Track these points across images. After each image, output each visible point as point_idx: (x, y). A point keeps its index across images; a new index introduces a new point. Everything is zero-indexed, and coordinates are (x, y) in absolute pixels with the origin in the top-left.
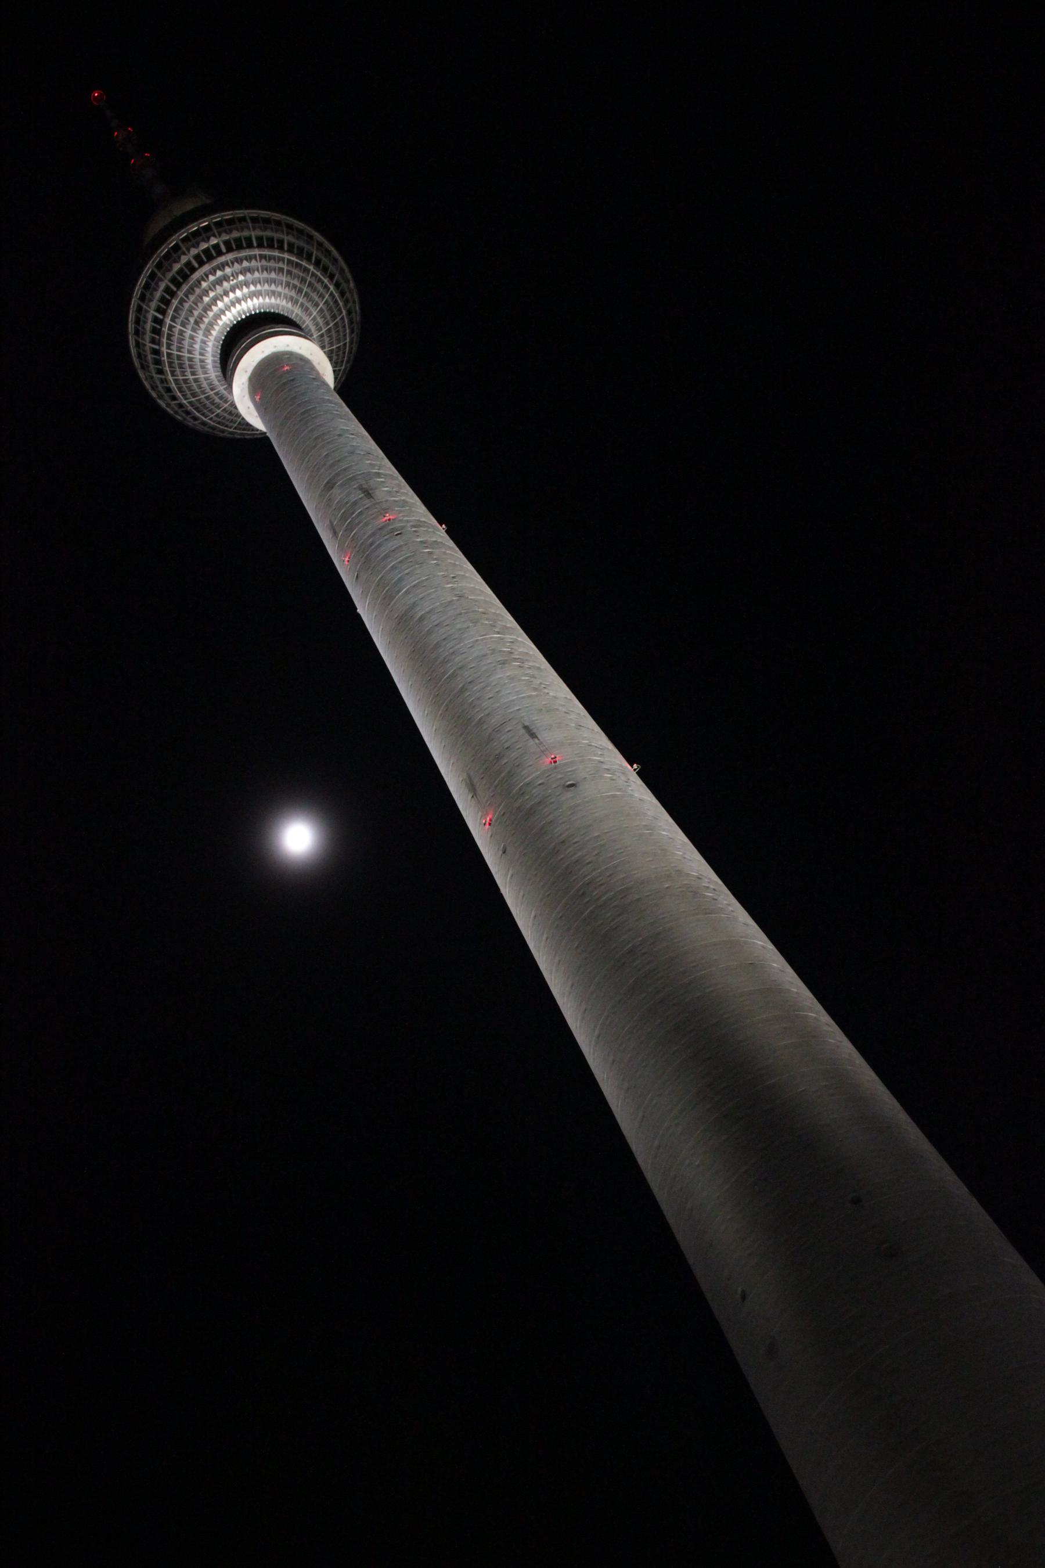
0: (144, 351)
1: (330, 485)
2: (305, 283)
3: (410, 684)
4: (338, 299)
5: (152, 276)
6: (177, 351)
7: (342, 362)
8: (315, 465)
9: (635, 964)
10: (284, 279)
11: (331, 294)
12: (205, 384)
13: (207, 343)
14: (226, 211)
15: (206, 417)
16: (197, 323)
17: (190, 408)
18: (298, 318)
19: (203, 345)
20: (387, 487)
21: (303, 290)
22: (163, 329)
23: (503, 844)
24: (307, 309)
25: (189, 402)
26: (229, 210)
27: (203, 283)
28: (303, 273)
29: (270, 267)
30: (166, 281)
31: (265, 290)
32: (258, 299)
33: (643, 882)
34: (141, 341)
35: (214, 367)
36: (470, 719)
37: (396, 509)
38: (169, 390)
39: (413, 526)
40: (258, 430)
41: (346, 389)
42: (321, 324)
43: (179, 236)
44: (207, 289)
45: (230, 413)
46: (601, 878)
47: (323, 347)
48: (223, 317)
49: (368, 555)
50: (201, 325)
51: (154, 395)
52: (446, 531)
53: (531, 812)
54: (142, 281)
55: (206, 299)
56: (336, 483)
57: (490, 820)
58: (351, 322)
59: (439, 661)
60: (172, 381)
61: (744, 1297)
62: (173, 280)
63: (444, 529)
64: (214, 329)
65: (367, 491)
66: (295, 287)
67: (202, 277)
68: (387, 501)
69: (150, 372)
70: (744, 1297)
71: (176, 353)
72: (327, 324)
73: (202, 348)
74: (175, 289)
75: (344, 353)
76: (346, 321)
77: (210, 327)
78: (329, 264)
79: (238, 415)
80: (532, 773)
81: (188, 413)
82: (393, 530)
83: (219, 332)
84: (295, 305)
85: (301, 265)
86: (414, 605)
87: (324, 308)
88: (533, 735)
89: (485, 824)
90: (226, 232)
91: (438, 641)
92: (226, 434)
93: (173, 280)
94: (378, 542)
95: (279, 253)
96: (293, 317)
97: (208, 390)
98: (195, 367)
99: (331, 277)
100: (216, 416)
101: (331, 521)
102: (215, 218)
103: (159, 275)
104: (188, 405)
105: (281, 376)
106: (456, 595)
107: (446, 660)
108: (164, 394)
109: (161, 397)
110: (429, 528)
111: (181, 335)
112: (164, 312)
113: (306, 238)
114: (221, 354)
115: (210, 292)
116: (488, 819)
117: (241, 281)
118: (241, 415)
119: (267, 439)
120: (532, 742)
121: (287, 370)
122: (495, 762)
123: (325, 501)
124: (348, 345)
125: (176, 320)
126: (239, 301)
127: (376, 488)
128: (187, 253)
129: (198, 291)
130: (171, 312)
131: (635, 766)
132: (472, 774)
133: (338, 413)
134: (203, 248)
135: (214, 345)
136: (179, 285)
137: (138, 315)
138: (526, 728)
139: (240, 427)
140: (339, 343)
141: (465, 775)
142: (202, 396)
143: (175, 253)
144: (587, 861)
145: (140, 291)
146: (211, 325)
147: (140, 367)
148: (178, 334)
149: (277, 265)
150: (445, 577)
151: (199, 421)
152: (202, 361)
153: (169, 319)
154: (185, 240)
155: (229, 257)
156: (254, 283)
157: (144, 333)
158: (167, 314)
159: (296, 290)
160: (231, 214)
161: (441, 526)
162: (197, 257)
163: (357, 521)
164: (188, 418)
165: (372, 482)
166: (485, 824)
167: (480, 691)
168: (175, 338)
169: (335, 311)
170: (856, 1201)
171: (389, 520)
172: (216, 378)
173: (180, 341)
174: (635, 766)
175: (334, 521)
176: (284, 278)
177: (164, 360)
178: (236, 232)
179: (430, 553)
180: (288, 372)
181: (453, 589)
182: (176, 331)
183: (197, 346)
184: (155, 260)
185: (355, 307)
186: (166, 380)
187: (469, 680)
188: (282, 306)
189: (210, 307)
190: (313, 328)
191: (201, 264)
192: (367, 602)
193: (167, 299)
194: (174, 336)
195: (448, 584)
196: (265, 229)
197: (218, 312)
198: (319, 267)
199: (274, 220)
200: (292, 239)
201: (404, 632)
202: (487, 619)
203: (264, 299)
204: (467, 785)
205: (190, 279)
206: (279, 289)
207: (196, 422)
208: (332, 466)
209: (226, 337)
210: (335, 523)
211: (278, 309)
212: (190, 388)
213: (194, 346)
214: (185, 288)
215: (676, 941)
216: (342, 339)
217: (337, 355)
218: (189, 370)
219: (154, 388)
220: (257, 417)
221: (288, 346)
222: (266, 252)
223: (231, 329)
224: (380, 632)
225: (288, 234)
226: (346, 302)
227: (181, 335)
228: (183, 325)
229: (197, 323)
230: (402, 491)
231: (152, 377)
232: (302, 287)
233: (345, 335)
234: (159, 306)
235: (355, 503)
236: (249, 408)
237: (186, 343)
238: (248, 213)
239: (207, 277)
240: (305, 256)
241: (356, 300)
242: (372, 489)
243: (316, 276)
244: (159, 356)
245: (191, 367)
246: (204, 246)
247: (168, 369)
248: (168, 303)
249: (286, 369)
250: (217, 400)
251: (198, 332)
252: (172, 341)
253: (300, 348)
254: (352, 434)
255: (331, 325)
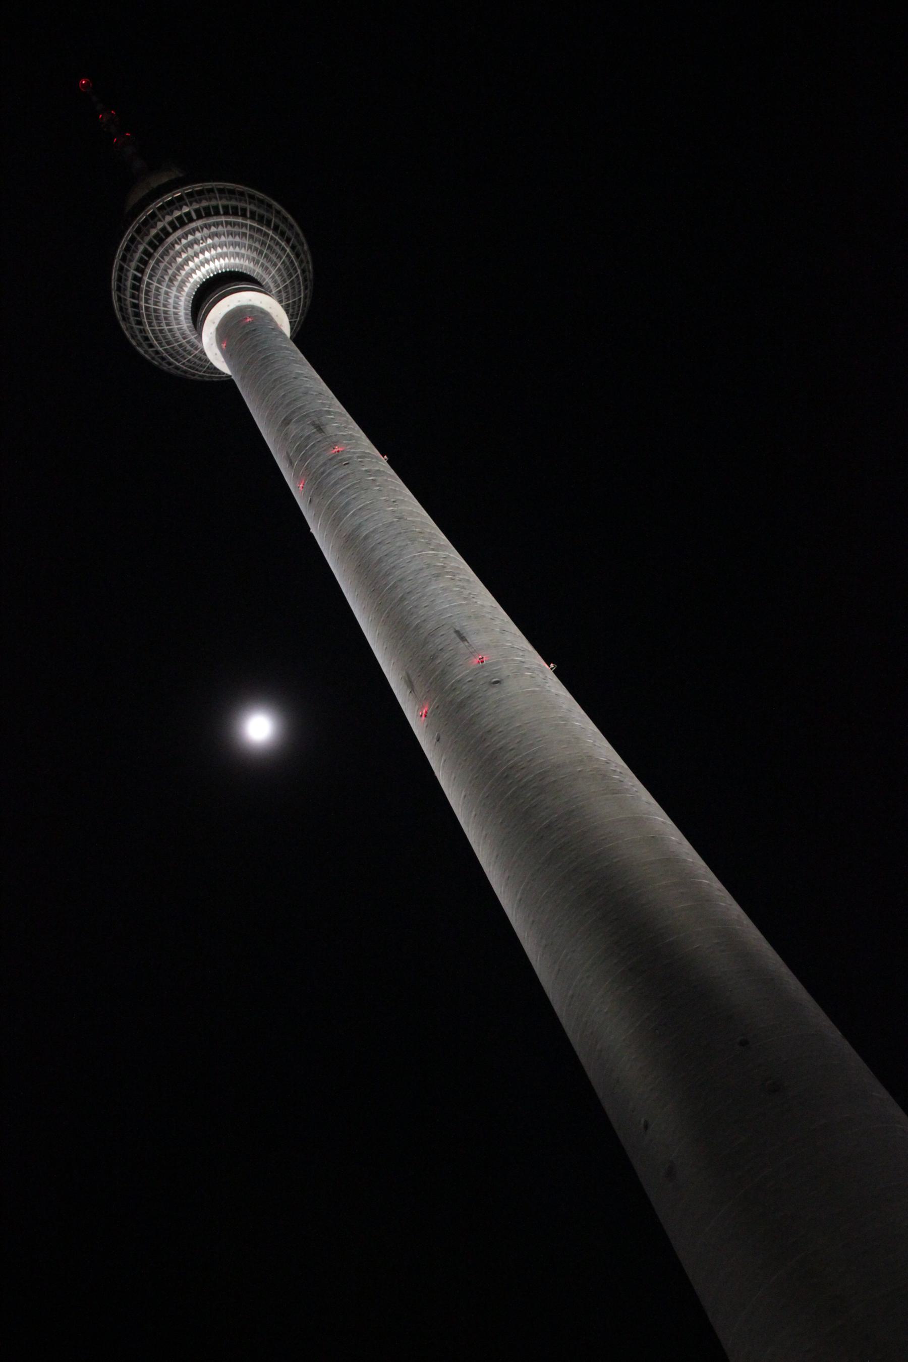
0: (125, 304)
1: (287, 422)
2: (265, 246)
3: (356, 594)
4: (294, 260)
5: (132, 240)
6: (154, 305)
7: (297, 314)
8: (274, 404)
9: (552, 837)
10: (247, 243)
11: (288, 256)
12: (178, 333)
13: (180, 298)
14: (196, 183)
15: (179, 362)
16: (171, 280)
17: (165, 354)
18: (259, 277)
19: (176, 299)
20: (336, 423)
21: (263, 252)
22: (142, 286)
23: (437, 733)
24: (267, 269)
25: (164, 350)
26: (199, 183)
27: (176, 246)
28: (263, 237)
29: (235, 232)
30: (144, 244)
31: (230, 252)
32: (224, 259)
33: (558, 766)
34: (122, 296)
35: (186, 319)
36: (408, 624)
37: (344, 442)
38: (147, 339)
39: (359, 457)
40: (224, 373)
41: (300, 338)
42: (279, 282)
43: (155, 205)
44: (180, 251)
45: (200, 359)
46: (522, 763)
47: (280, 302)
48: (193, 275)
49: (320, 482)
50: (175, 283)
51: (134, 343)
52: (387, 461)
53: (461, 705)
54: (123, 244)
55: (179, 260)
56: (292, 419)
57: (426, 712)
58: (305, 280)
59: (381, 574)
60: (150, 331)
61: (646, 1127)
62: (151, 243)
63: (385, 459)
64: (186, 286)
65: (319, 426)
66: (256, 249)
67: (176, 241)
68: (336, 435)
69: (130, 324)
70: (646, 1127)
71: (153, 306)
72: (284, 281)
73: (176, 303)
74: (152, 251)
75: (299, 307)
76: (301, 279)
77: (183, 284)
78: (286, 229)
79: (207, 361)
80: (462, 672)
81: (163, 359)
82: (341, 461)
83: (190, 288)
84: (256, 265)
85: (261, 230)
86: (360, 525)
87: (282, 267)
88: (463, 639)
89: (421, 716)
90: (196, 201)
91: (381, 557)
92: (196, 377)
93: (151, 243)
94: (328, 471)
95: (242, 219)
96: (254, 275)
97: (181, 339)
98: (169, 318)
99: (288, 241)
100: (188, 361)
101: (287, 453)
102: (187, 189)
103: (138, 239)
104: (163, 352)
105: (244, 327)
106: (396, 517)
107: (387, 574)
108: (143, 342)
109: (140, 345)
110: (372, 458)
111: (158, 291)
112: (142, 271)
113: (265, 207)
114: (192, 308)
115: (182, 253)
116: (424, 712)
117: (209, 244)
118: (209, 361)
119: (232, 381)
120: (462, 645)
121: (249, 321)
122: (430, 662)
123: (282, 435)
124: (302, 300)
125: (153, 278)
126: (207, 261)
127: (327, 424)
128: (162, 219)
129: (172, 253)
130: (148, 271)
131: (552, 665)
132: (410, 672)
133: (294, 359)
134: (176, 216)
135: (186, 300)
136: (155, 248)
137: (120, 273)
138: (457, 632)
139: (209, 371)
140: (295, 298)
141: (404, 673)
142: (176, 344)
143: (152, 220)
144: (510, 748)
145: (122, 253)
146: (183, 282)
147: (121, 319)
148: (155, 290)
149: (241, 230)
150: (386, 501)
151: (173, 366)
152: (175, 314)
153: (147, 277)
154: (161, 208)
155: (199, 223)
156: (221, 246)
157: (125, 290)
158: (145, 272)
159: (257, 252)
160: (201, 186)
161: (383, 457)
162: (171, 224)
163: (310, 453)
164: (163, 363)
165: (323, 419)
166: (421, 716)
167: (417, 600)
168: (152, 294)
169: (291, 271)
170: (744, 1043)
171: (338, 451)
172: (188, 328)
173: (157, 296)
174: (552, 665)
175: (291, 453)
176: (247, 242)
177: (143, 313)
178: (205, 201)
179: (373, 480)
180: (250, 323)
181: (393, 511)
182: (153, 287)
183: (171, 301)
184: (134, 225)
185: (308, 267)
186: (144, 330)
187: (408, 590)
188: (245, 266)
189: (183, 266)
190: (272, 285)
191: (175, 229)
192: (319, 523)
193: (145, 260)
194: (152, 292)
195: (389, 507)
196: (231, 199)
197: (190, 271)
198: (277, 232)
199: (238, 191)
200: (254, 208)
201: (351, 549)
202: (423, 538)
203: (229, 259)
204: (406, 682)
205: (165, 242)
206: (243, 251)
207: (171, 367)
208: (288, 405)
209: (196, 292)
210: (291, 455)
211: (242, 268)
212: (165, 337)
213: (169, 300)
214: (161, 250)
215: (587, 817)
216: (297, 295)
217: (293, 309)
218: (164, 322)
219: (134, 337)
220: (223, 362)
221: (250, 300)
222: (231, 219)
223: (201, 285)
224: (330, 549)
225: (250, 203)
226: (301, 262)
227: (158, 291)
228: (159, 282)
229: (171, 280)
230: (350, 426)
231: (132, 328)
232: (263, 249)
233: (300, 291)
234: (138, 266)
235: (309, 437)
236: (216, 354)
237: (162, 298)
238: (216, 185)
239: (180, 241)
240: (265, 222)
241: (310, 260)
242: (323, 425)
243: (275, 240)
244: (139, 309)
245: (166, 319)
246: (177, 213)
247: (146, 321)
248: (146, 263)
249: (248, 320)
250: (189, 348)
251: (172, 288)
252: (149, 296)
253: (261, 302)
254: (306, 377)
255: (288, 282)
